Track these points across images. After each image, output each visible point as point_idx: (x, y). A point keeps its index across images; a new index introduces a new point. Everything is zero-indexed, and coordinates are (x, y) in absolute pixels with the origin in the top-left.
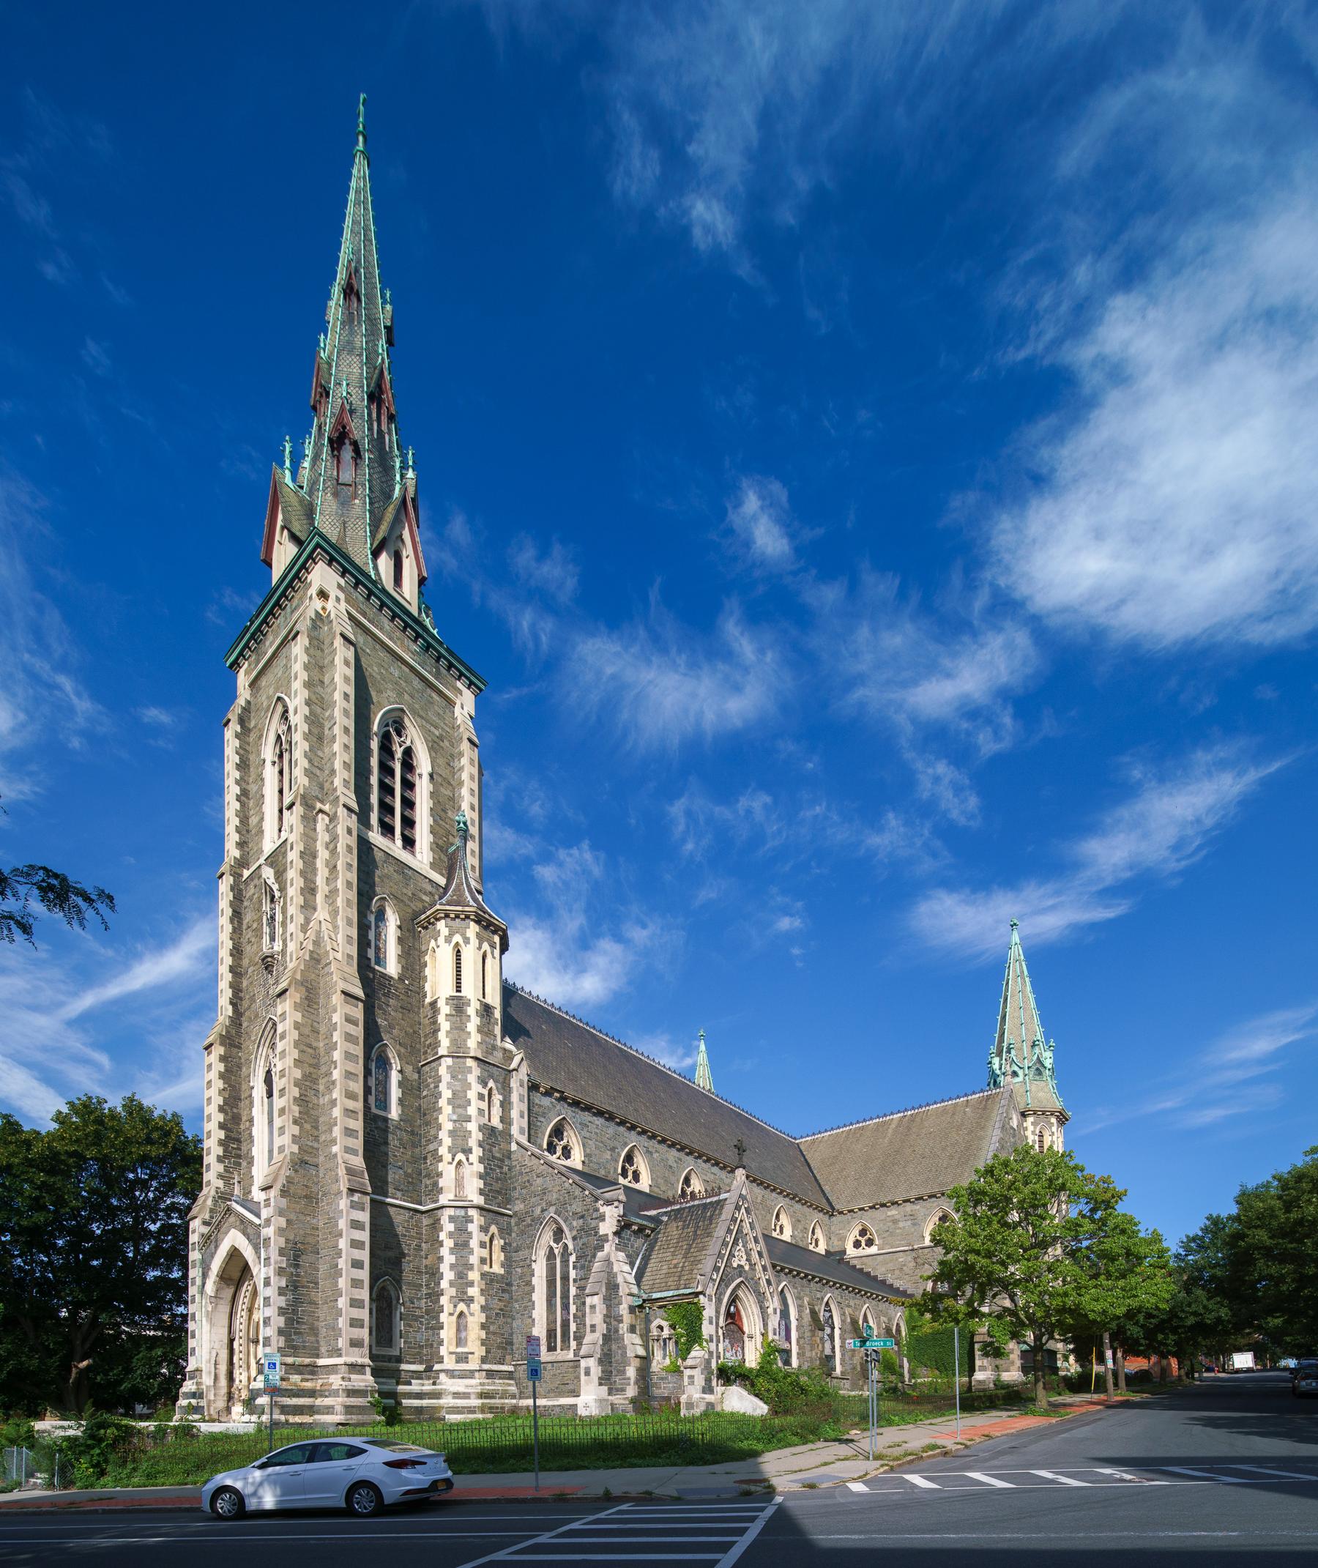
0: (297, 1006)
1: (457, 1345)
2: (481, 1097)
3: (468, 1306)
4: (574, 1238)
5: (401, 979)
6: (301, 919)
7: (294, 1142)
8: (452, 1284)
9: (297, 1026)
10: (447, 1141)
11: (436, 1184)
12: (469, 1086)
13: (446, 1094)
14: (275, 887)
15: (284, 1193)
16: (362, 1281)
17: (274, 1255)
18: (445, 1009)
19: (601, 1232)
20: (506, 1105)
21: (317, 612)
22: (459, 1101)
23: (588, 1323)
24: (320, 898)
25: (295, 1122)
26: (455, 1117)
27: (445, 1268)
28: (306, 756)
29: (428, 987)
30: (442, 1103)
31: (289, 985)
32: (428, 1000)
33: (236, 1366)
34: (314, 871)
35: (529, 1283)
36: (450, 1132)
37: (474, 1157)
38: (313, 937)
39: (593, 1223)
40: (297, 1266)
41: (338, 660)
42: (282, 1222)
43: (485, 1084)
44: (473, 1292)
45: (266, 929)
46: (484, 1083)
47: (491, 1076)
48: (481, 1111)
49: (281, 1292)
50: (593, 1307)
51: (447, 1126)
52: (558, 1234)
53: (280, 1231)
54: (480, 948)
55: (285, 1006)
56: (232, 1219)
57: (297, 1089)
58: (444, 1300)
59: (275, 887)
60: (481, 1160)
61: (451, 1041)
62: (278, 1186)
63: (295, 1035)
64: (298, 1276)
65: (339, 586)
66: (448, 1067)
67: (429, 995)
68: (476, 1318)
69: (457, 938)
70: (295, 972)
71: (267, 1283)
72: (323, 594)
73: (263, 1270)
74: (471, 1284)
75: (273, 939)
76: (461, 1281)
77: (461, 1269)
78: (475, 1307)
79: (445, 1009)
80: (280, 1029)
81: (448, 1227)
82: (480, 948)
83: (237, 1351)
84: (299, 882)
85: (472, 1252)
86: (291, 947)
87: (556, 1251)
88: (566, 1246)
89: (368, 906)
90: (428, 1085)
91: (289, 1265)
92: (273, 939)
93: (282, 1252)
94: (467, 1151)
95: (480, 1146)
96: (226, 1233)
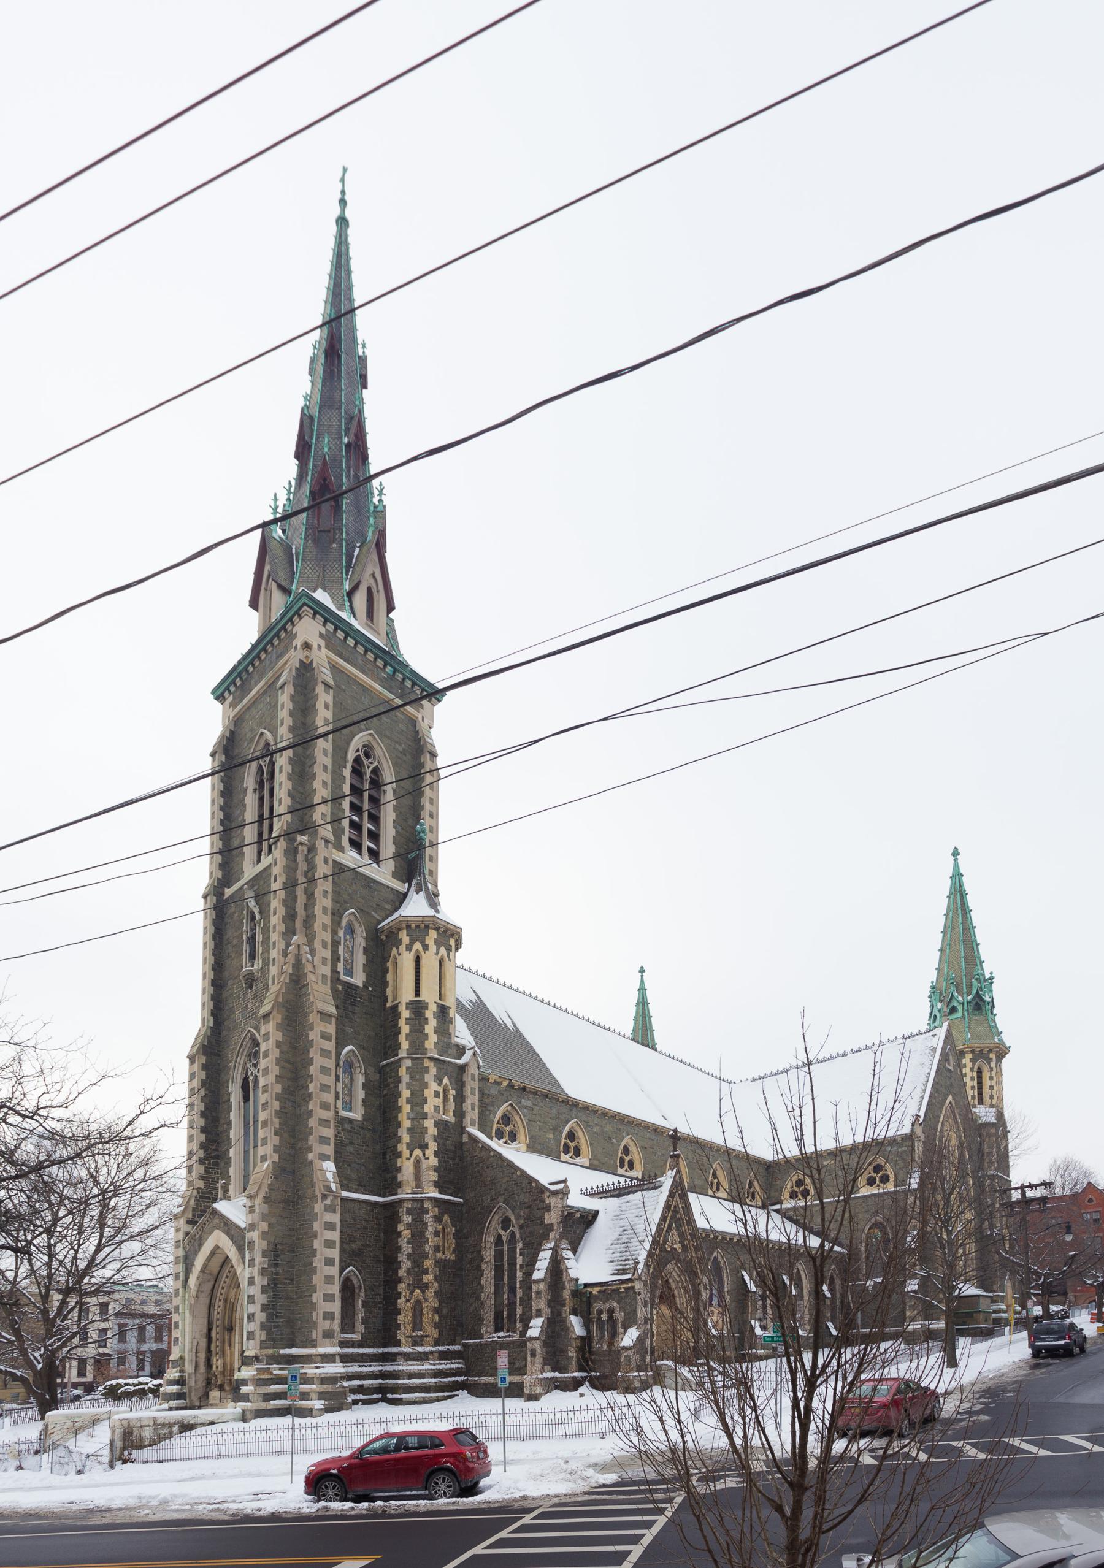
0: (279, 1027)
1: (414, 1330)
2: (437, 1094)
3: (423, 1292)
4: (521, 1227)
5: (365, 987)
6: (282, 945)
7: (275, 1152)
8: (408, 1272)
9: (279, 1045)
10: (406, 1138)
11: (395, 1178)
12: (426, 1086)
13: (406, 1093)
14: (256, 911)
15: (266, 1200)
16: (333, 1277)
17: (258, 1258)
18: (405, 1014)
19: (547, 1222)
20: (460, 1098)
21: (301, 661)
22: (418, 1100)
23: (534, 1308)
24: (299, 923)
25: (276, 1134)
26: (412, 1116)
27: (403, 1257)
28: (289, 795)
29: (389, 991)
30: (402, 1101)
31: (273, 1007)
32: (389, 1005)
33: (214, 1353)
34: (295, 899)
35: (479, 1268)
36: (408, 1129)
37: (429, 1152)
38: (292, 961)
39: (539, 1213)
40: (276, 1265)
41: (320, 705)
42: (264, 1226)
43: (440, 1083)
44: (428, 1278)
45: (246, 948)
46: (439, 1080)
47: (446, 1074)
48: (436, 1108)
49: (264, 1290)
50: (538, 1293)
51: (407, 1124)
52: (506, 1223)
53: (264, 1235)
54: (437, 953)
55: (270, 1027)
56: (216, 1221)
57: (278, 1103)
58: (402, 1287)
59: (256, 911)
60: (436, 1154)
61: (410, 1045)
62: (262, 1195)
63: (276, 1053)
64: (277, 1274)
65: (321, 635)
66: (408, 1068)
67: (390, 999)
68: (431, 1300)
69: (417, 946)
70: (277, 996)
71: (251, 1281)
72: (307, 646)
73: (248, 1270)
74: (426, 1272)
75: (253, 957)
76: (418, 1270)
77: (418, 1257)
78: (431, 1293)
79: (405, 1014)
80: (263, 1047)
81: (407, 1219)
82: (437, 953)
83: (214, 1339)
84: (281, 911)
85: (427, 1241)
86: (273, 970)
87: (504, 1239)
88: (513, 1233)
89: (339, 924)
90: (388, 1085)
91: (270, 1266)
92: (253, 957)
93: (264, 1254)
94: (424, 1147)
95: (435, 1141)
96: (211, 1233)
